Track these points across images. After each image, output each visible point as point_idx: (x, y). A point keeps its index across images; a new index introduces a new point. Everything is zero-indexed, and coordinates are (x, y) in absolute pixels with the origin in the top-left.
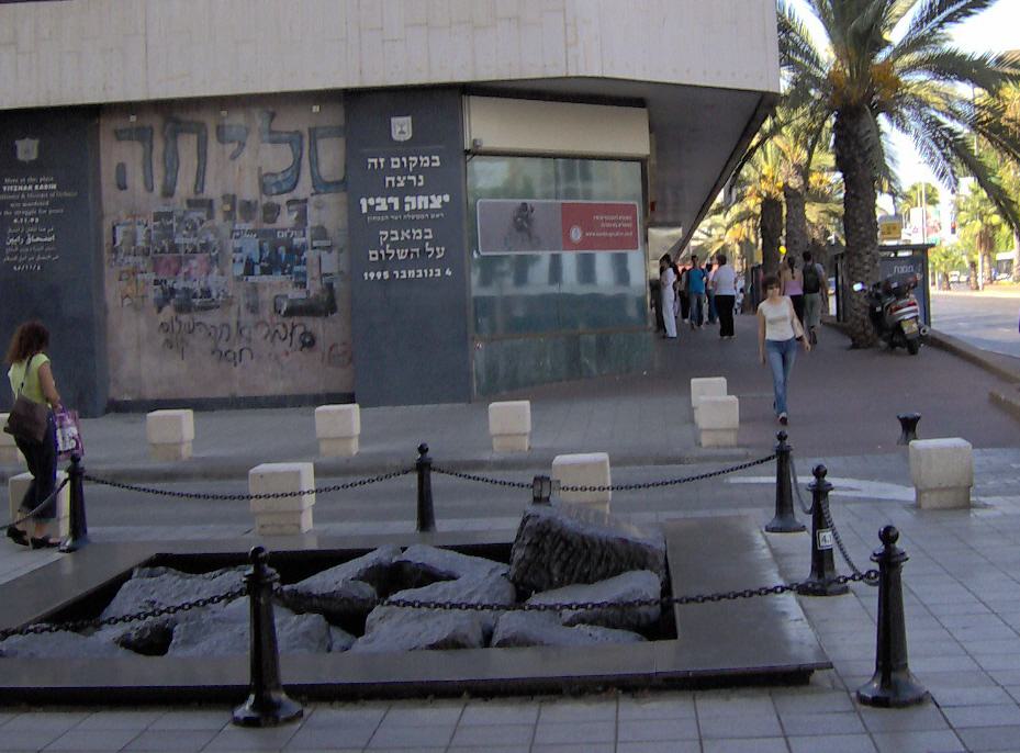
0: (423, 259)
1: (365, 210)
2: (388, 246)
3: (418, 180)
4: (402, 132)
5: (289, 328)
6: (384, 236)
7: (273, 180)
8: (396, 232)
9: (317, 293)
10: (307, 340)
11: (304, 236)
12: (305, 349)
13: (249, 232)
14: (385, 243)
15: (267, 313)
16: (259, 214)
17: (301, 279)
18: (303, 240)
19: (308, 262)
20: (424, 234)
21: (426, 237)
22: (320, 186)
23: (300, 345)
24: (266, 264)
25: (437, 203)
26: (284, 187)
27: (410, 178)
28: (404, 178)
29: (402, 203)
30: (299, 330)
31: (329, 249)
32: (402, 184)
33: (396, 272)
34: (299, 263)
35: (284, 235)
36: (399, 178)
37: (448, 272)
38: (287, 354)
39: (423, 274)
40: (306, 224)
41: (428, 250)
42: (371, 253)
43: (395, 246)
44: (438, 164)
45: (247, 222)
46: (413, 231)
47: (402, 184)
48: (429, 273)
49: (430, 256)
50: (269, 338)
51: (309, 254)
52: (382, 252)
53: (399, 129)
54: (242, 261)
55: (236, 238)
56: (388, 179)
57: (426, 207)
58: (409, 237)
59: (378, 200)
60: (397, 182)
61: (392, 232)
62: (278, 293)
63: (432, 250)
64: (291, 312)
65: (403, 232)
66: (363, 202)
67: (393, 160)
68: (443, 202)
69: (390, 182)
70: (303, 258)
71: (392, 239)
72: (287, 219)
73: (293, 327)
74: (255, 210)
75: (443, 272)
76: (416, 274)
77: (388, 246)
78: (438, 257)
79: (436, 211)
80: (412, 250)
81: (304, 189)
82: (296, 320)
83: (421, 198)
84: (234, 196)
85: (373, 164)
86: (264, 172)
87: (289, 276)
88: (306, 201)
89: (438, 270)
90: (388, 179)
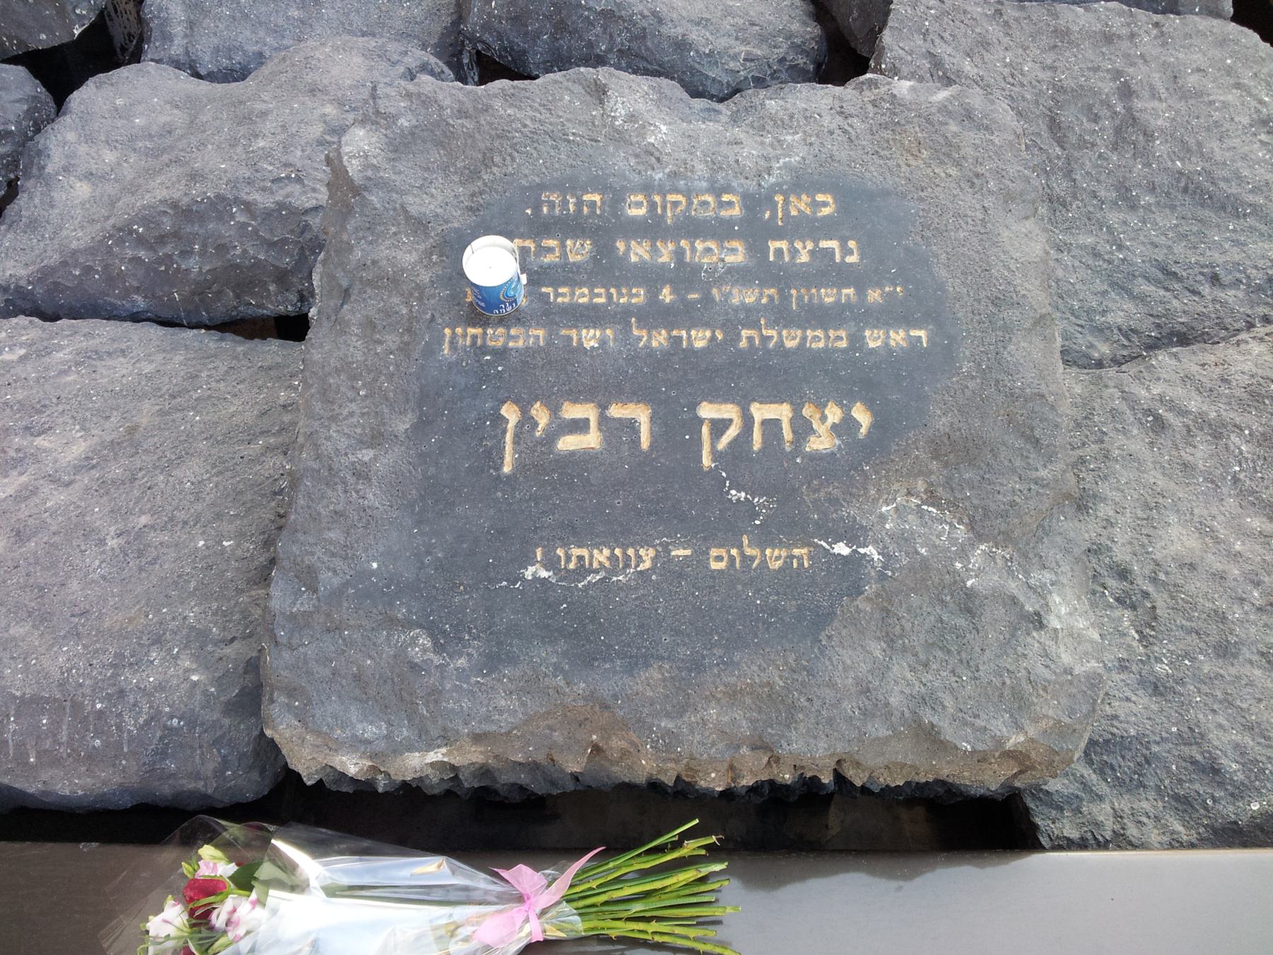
3: (847, 252)
6: (719, 427)
27: (824, 244)
28: (810, 246)
32: (804, 258)
36: (798, 245)
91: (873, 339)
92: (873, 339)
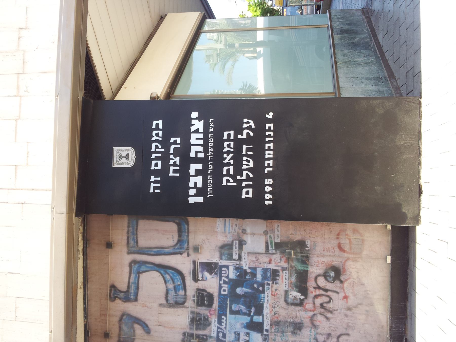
0: (257, 141)
1: (200, 199)
2: (239, 178)
4: (127, 157)
5: (318, 292)
6: (228, 181)
7: (172, 294)
8: (225, 169)
9: (284, 259)
10: (332, 274)
11: (227, 267)
12: (342, 278)
13: (220, 322)
14: (235, 180)
15: (302, 315)
16: (203, 311)
17: (269, 274)
18: (231, 268)
19: (253, 265)
20: (229, 139)
21: (232, 137)
22: (181, 246)
23: (337, 283)
24: (253, 310)
25: (198, 125)
26: (179, 282)
27: (172, 151)
28: (172, 157)
29: (197, 160)
30: (322, 282)
31: (242, 244)
33: (267, 170)
34: (254, 275)
35: (225, 287)
36: (171, 162)
37: (270, 116)
38: (346, 297)
39: (269, 142)
40: (216, 264)
41: (245, 136)
42: (244, 196)
43: (238, 170)
44: (160, 122)
45: (210, 324)
46: (225, 150)
47: (178, 160)
48: (269, 136)
49: (252, 134)
50: (329, 315)
51: (246, 264)
52: (244, 184)
53: (124, 160)
54: (248, 334)
55: (224, 336)
56: (171, 174)
57: (201, 136)
58: (231, 155)
59: (191, 184)
60: (175, 164)
61: (225, 172)
62: (282, 300)
63: (245, 132)
64: (303, 290)
65: (225, 161)
66: (192, 200)
67: (153, 168)
68: (199, 119)
69: (175, 171)
70: (249, 271)
71: (232, 173)
72: (211, 283)
73: (319, 288)
74: (198, 314)
75: (269, 121)
76: (269, 149)
77: (239, 178)
78: (253, 126)
79: (206, 126)
80: (244, 153)
81: (182, 263)
82: (311, 284)
83: (193, 141)
84: (184, 334)
85: (155, 188)
86: (164, 302)
87: (266, 287)
88: (194, 262)
89: (267, 126)
90: (171, 174)
91: (211, 130)
92: (211, 130)
